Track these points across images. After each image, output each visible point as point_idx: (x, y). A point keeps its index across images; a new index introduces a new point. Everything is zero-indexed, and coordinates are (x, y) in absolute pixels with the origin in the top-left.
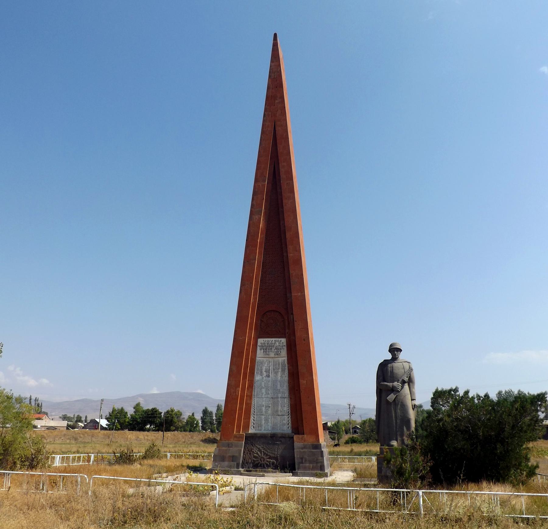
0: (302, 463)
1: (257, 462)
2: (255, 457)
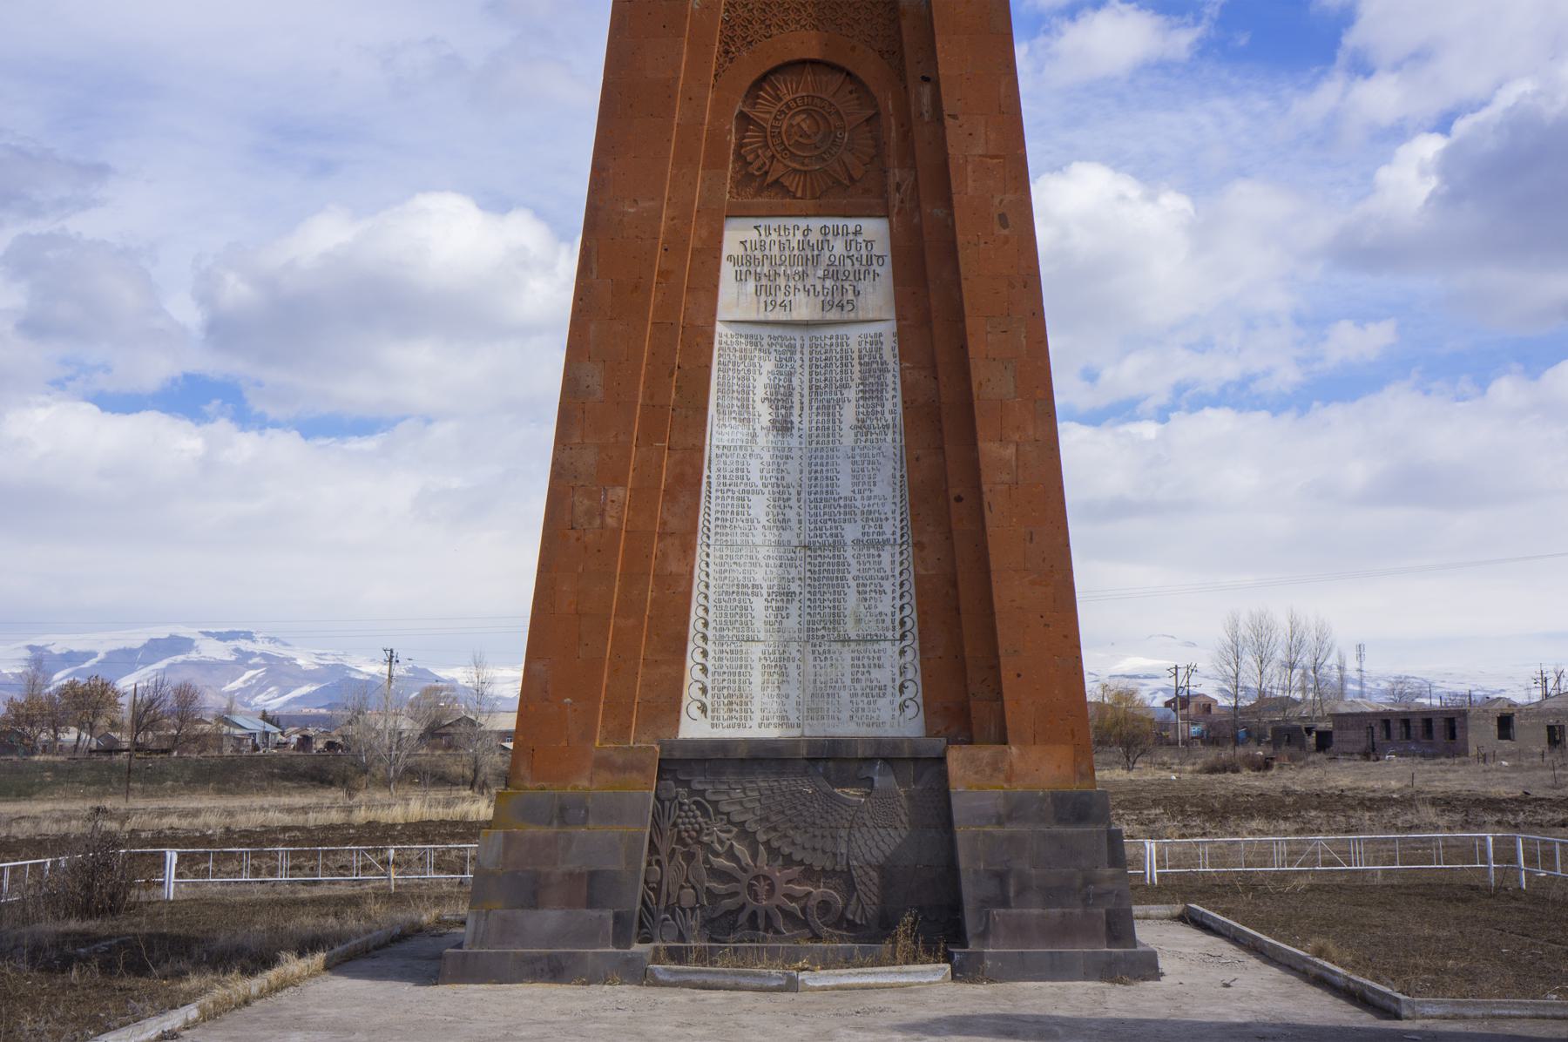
1: (728, 903)
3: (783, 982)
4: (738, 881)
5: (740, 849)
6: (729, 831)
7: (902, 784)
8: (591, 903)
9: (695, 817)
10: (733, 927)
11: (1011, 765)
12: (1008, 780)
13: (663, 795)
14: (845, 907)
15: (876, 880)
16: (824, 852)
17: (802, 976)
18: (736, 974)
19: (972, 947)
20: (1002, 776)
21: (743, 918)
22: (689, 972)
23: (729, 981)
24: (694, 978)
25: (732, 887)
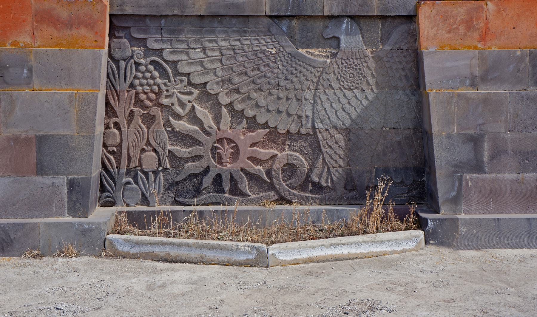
0: (478, 167)
1: (192, 167)
2: (178, 137)
3: (252, 257)
4: (201, 144)
5: (203, 112)
6: (190, 93)
7: (368, 44)
8: (41, 170)
9: (153, 78)
10: (198, 191)
11: (486, 23)
12: (483, 39)
13: (117, 55)
14: (311, 170)
15: (342, 144)
16: (289, 115)
17: (274, 249)
18: (202, 247)
19: (444, 213)
20: (476, 35)
21: (208, 181)
22: (150, 244)
23: (194, 254)
24: (156, 250)
25: (195, 150)
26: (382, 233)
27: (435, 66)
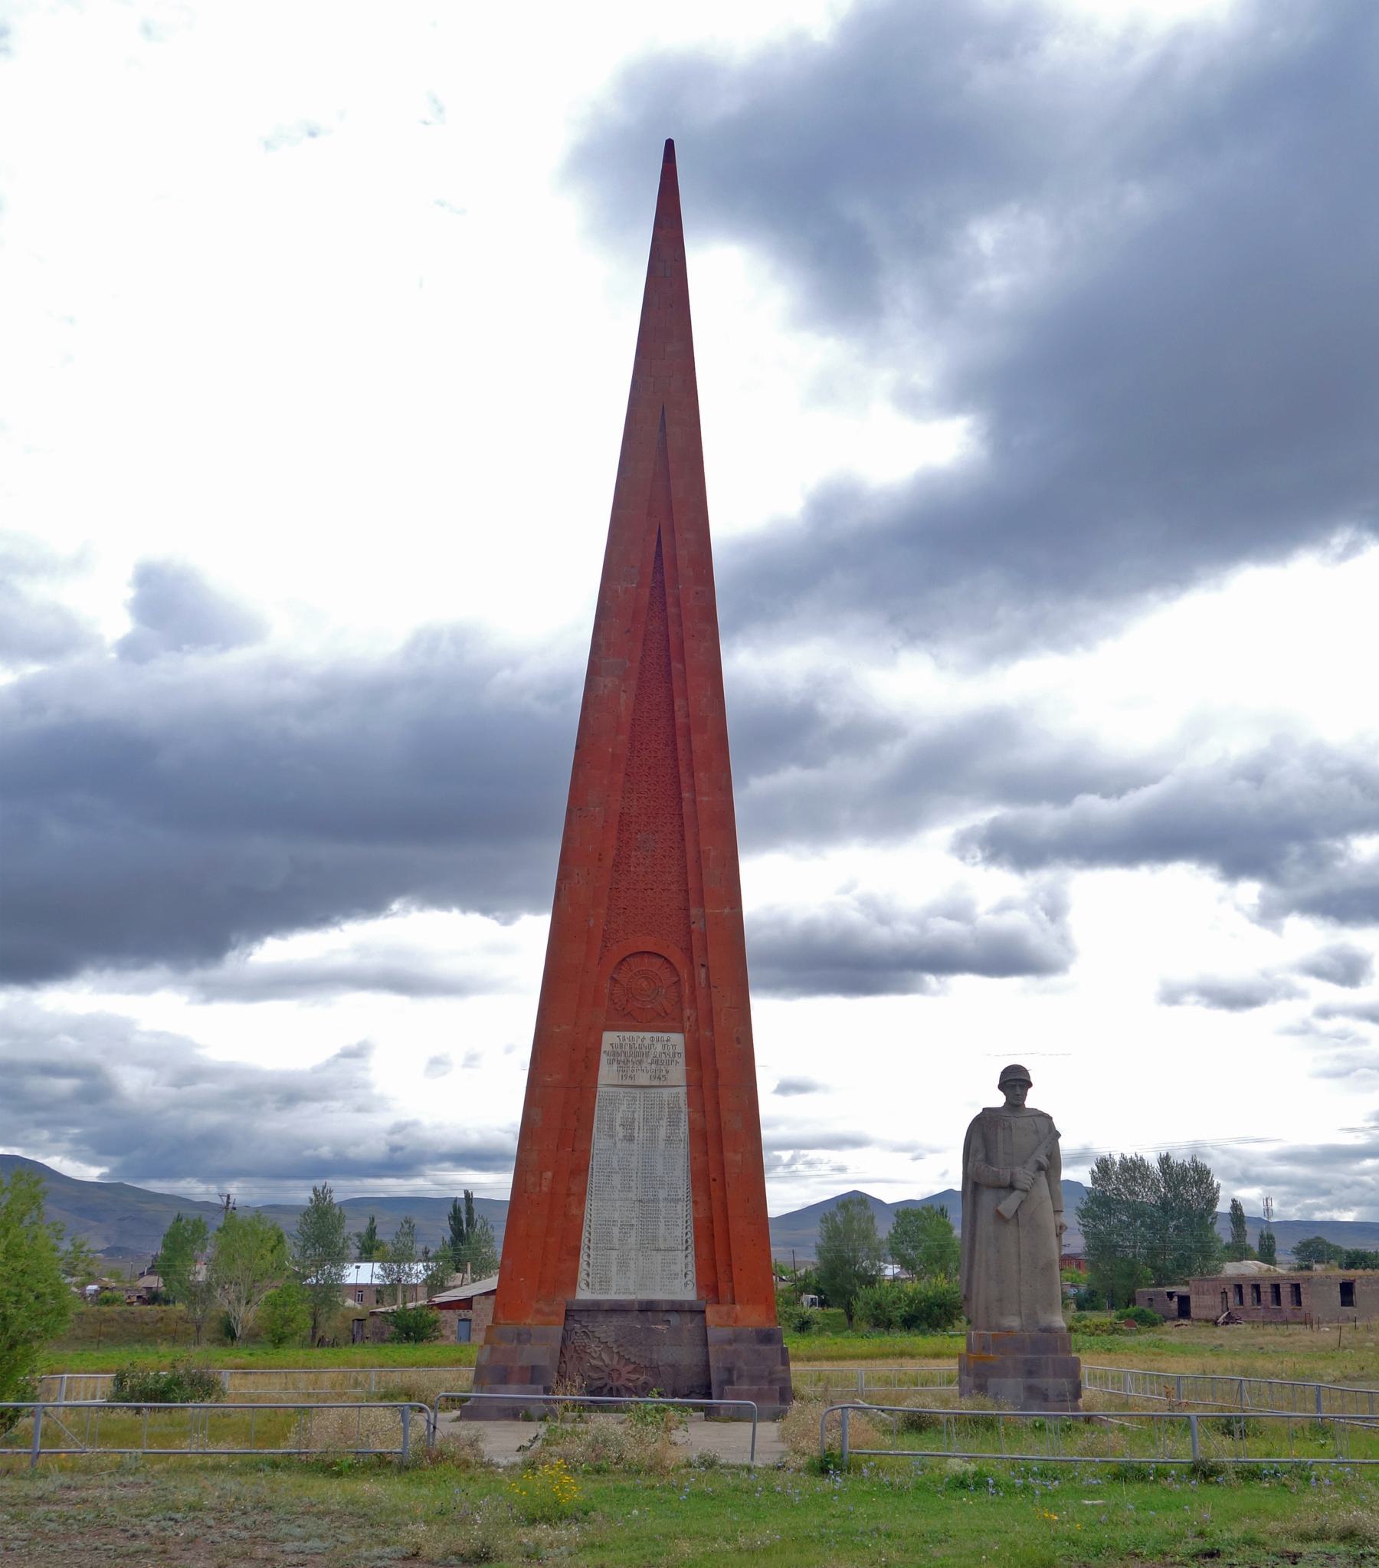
2: (596, 1368)
25: (601, 1375)
26: (344, 1349)
27: (714, 1334)
